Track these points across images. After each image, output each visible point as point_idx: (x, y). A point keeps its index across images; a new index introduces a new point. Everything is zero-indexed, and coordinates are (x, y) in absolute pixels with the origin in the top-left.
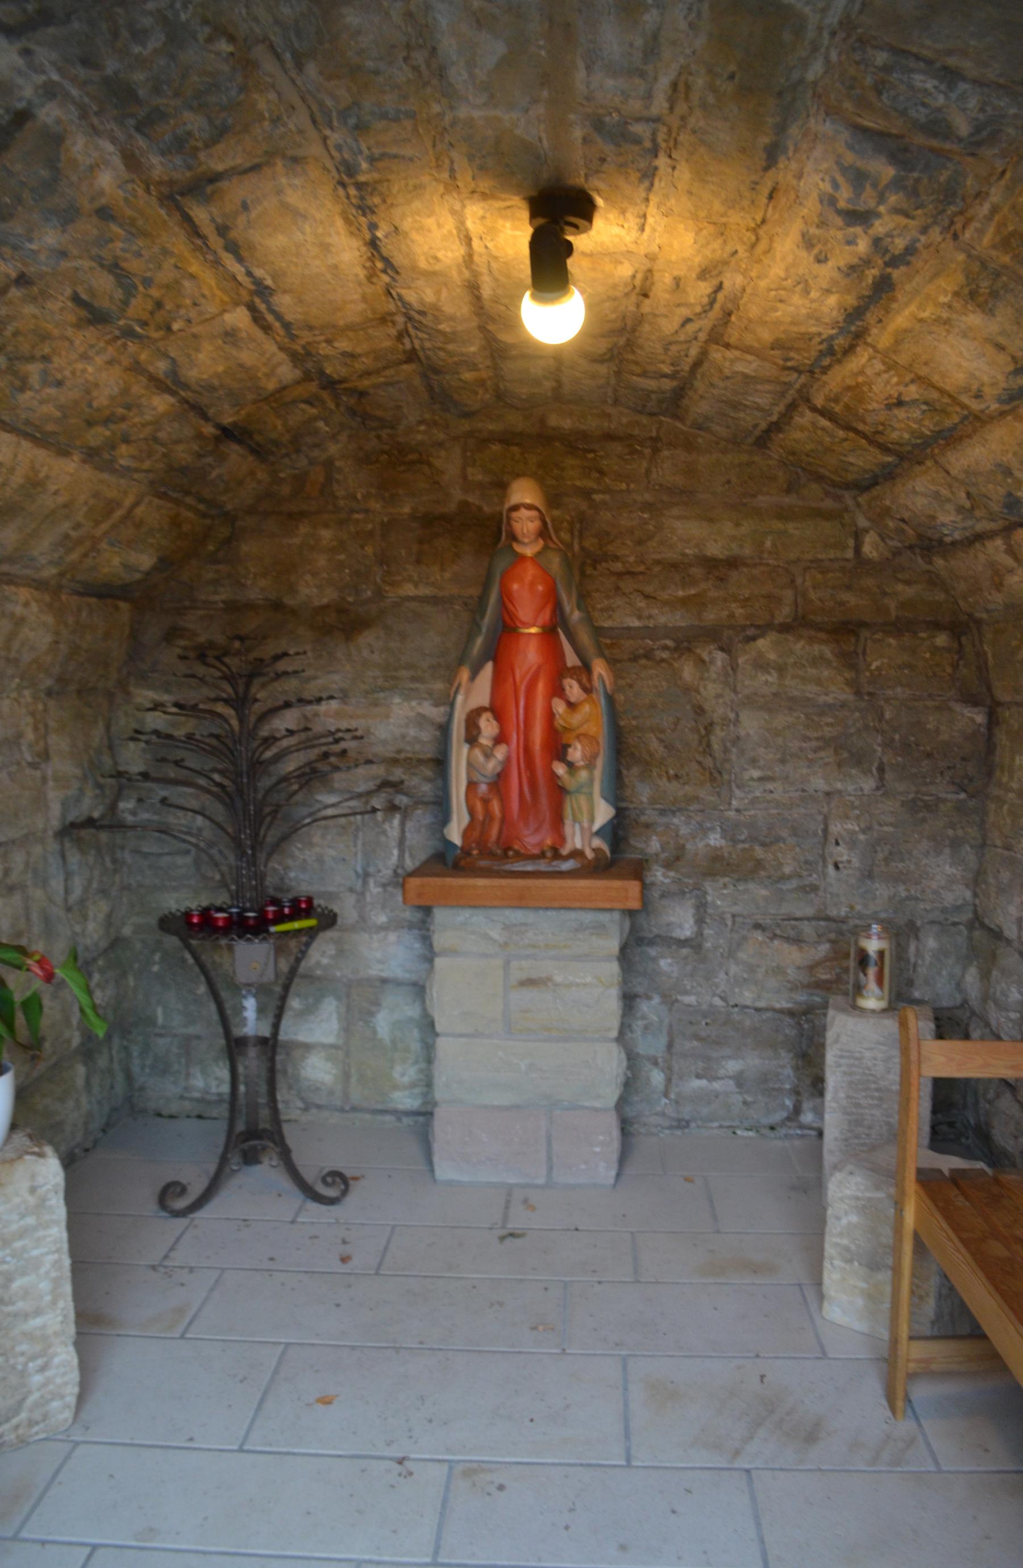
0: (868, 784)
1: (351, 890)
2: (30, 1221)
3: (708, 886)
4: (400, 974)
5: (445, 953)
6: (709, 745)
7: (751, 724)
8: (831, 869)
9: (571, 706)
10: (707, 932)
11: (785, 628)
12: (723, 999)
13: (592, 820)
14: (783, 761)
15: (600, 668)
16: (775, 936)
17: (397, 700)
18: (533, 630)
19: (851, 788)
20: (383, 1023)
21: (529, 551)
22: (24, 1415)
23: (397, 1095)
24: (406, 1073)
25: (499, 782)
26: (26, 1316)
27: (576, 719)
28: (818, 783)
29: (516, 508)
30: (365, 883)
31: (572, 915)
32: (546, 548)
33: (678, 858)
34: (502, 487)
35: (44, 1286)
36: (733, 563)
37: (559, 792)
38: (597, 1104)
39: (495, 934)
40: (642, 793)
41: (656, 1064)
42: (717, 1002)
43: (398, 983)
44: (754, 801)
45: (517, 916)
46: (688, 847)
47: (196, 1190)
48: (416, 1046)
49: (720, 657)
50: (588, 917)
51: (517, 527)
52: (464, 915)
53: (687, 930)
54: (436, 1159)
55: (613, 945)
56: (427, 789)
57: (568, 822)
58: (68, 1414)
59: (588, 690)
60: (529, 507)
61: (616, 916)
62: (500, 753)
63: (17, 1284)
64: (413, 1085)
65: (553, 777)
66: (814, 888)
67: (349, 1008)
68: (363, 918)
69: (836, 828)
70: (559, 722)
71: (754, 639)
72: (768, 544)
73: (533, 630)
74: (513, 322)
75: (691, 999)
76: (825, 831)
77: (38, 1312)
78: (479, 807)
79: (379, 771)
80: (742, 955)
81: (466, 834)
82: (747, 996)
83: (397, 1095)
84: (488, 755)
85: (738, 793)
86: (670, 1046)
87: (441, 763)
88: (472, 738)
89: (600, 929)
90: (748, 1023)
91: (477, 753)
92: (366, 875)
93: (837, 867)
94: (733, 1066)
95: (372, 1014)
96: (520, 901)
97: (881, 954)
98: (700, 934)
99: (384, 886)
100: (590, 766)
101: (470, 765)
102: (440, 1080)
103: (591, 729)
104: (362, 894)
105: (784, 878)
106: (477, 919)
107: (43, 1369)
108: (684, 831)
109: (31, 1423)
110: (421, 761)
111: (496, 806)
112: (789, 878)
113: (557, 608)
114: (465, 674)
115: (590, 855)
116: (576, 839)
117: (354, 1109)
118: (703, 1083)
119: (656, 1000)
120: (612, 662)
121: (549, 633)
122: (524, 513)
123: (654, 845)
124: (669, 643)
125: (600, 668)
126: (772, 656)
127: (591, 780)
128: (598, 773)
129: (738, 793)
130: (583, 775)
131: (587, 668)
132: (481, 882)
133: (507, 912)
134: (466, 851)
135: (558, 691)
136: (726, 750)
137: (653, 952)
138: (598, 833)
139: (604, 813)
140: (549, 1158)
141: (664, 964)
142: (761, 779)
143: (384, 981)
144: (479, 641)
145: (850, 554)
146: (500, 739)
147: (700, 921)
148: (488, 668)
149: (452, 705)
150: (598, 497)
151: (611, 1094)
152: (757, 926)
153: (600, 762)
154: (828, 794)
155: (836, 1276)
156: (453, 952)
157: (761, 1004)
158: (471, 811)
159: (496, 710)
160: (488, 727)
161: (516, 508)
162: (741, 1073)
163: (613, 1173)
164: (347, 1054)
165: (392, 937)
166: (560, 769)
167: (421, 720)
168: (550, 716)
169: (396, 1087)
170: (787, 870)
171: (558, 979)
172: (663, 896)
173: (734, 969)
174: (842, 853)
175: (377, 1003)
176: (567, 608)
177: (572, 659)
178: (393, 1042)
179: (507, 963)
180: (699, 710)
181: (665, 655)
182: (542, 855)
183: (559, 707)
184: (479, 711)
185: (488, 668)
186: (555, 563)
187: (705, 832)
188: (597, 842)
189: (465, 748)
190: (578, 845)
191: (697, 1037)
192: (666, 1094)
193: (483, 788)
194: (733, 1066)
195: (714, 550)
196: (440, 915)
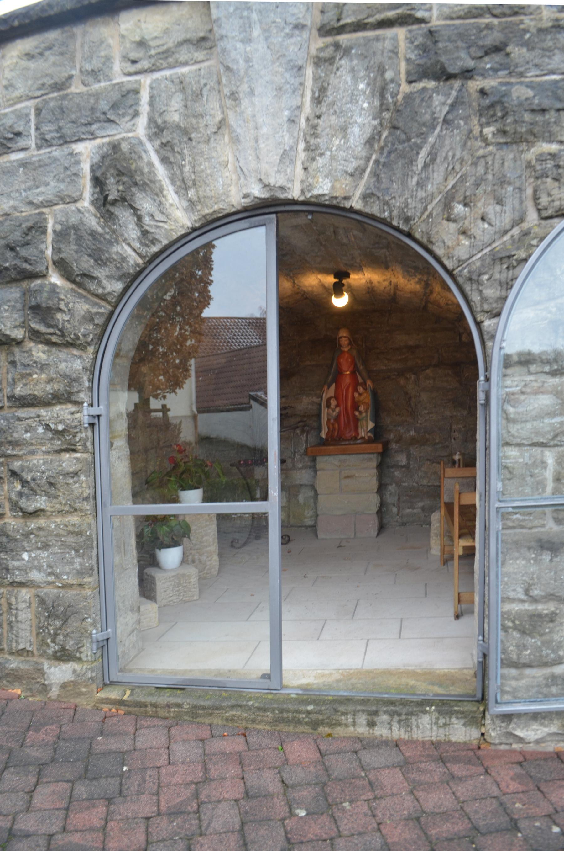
0: (465, 413)
1: (290, 457)
2: (208, 523)
3: (411, 448)
4: (307, 483)
5: (320, 470)
6: (410, 404)
7: (424, 397)
8: (453, 440)
9: (360, 395)
10: (411, 463)
11: (435, 366)
12: (417, 483)
13: (367, 427)
14: (435, 407)
15: (369, 383)
16: (433, 462)
17: (304, 397)
18: (348, 373)
19: (459, 414)
20: (301, 498)
21: (346, 350)
22: (205, 571)
23: (306, 520)
24: (309, 513)
25: (337, 418)
26: (206, 547)
27: (362, 398)
28: (448, 413)
29: (341, 337)
30: (295, 455)
31: (361, 456)
32: (351, 348)
33: (400, 440)
34: (338, 329)
35: (211, 540)
36: (417, 347)
37: (357, 421)
38: (370, 512)
39: (336, 463)
40: (387, 420)
41: (394, 505)
42: (415, 484)
43: (306, 485)
44: (426, 420)
45: (343, 457)
46: (404, 436)
47: (241, 542)
48: (312, 505)
49: (413, 377)
50: (366, 456)
51: (342, 343)
52: (326, 458)
53: (404, 462)
54: (318, 532)
55: (374, 464)
56: (315, 424)
57: (360, 429)
58: (216, 573)
59: (365, 389)
60: (345, 337)
61: (375, 455)
62: (337, 410)
63: (205, 538)
64: (311, 517)
65: (354, 416)
66: (447, 447)
67: (289, 494)
68: (294, 466)
69: (454, 427)
70: (356, 399)
71: (425, 370)
72: (429, 340)
73: (348, 373)
74: (330, 301)
75: (406, 484)
76: (451, 428)
77: (209, 546)
78: (331, 426)
79: (299, 419)
80: (423, 469)
81: (327, 435)
82: (425, 482)
83: (306, 520)
84: (333, 410)
85: (420, 418)
86: (399, 499)
87: (319, 416)
88: (328, 405)
89: (370, 460)
90: (425, 490)
91: (330, 411)
92: (295, 452)
93: (454, 439)
94: (420, 504)
95: (297, 495)
96: (344, 453)
97: (459, 460)
98: (408, 463)
99: (301, 455)
100: (366, 411)
101: (328, 414)
102: (319, 508)
103: (367, 400)
104: (294, 458)
105: (436, 444)
106: (331, 459)
107: (210, 560)
108: (402, 431)
109: (207, 573)
110: (313, 416)
111: (336, 426)
112: (438, 443)
113: (355, 366)
114: (326, 388)
115: (366, 438)
116: (362, 433)
117: (291, 526)
118: (411, 510)
119: (394, 485)
120: (373, 381)
121: (353, 373)
122: (343, 339)
123: (392, 436)
124: (396, 373)
125: (369, 383)
126: (431, 375)
127: (367, 416)
128: (369, 414)
129: (420, 418)
130: (364, 414)
131: (365, 383)
132: (331, 447)
133: (340, 456)
134: (327, 439)
135: (356, 390)
136: (416, 405)
137: (392, 470)
138: (370, 431)
139: (371, 425)
140: (355, 530)
141: (396, 473)
142: (428, 413)
143: (301, 485)
144: (330, 377)
145: (457, 341)
146: (337, 406)
147: (408, 459)
148: (334, 385)
149: (322, 397)
150: (371, 330)
151: (375, 509)
152: (428, 460)
153: (369, 410)
154: (451, 417)
155: (434, 542)
156: (323, 469)
157: (430, 484)
158: (329, 428)
159: (336, 397)
160: (333, 403)
161: (341, 337)
162: (423, 506)
163: (376, 533)
164: (289, 509)
165: (304, 471)
166: (357, 413)
167: (313, 403)
168: (353, 398)
169: (305, 518)
170: (437, 441)
171: (357, 475)
172: (395, 452)
173: (420, 474)
174: (456, 435)
175: (299, 492)
176: (358, 365)
177: (360, 380)
178: (305, 504)
179: (340, 472)
180: (406, 393)
181: (394, 377)
182: (351, 439)
183: (356, 395)
184: (331, 398)
185: (334, 385)
186: (354, 353)
187: (409, 431)
188: (369, 434)
189: (326, 410)
190: (363, 435)
191: (407, 495)
192: (398, 515)
193: (332, 421)
194: (420, 504)
195: (411, 343)
196: (319, 459)
